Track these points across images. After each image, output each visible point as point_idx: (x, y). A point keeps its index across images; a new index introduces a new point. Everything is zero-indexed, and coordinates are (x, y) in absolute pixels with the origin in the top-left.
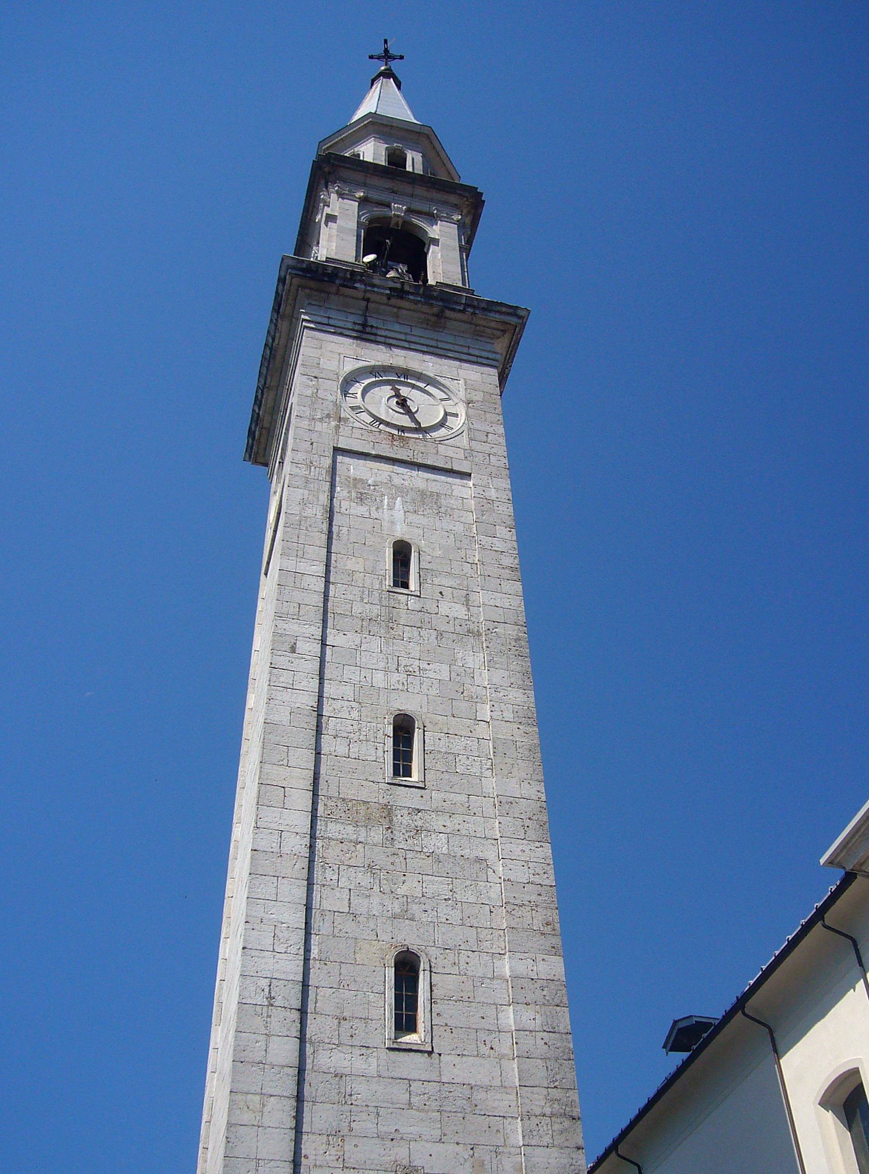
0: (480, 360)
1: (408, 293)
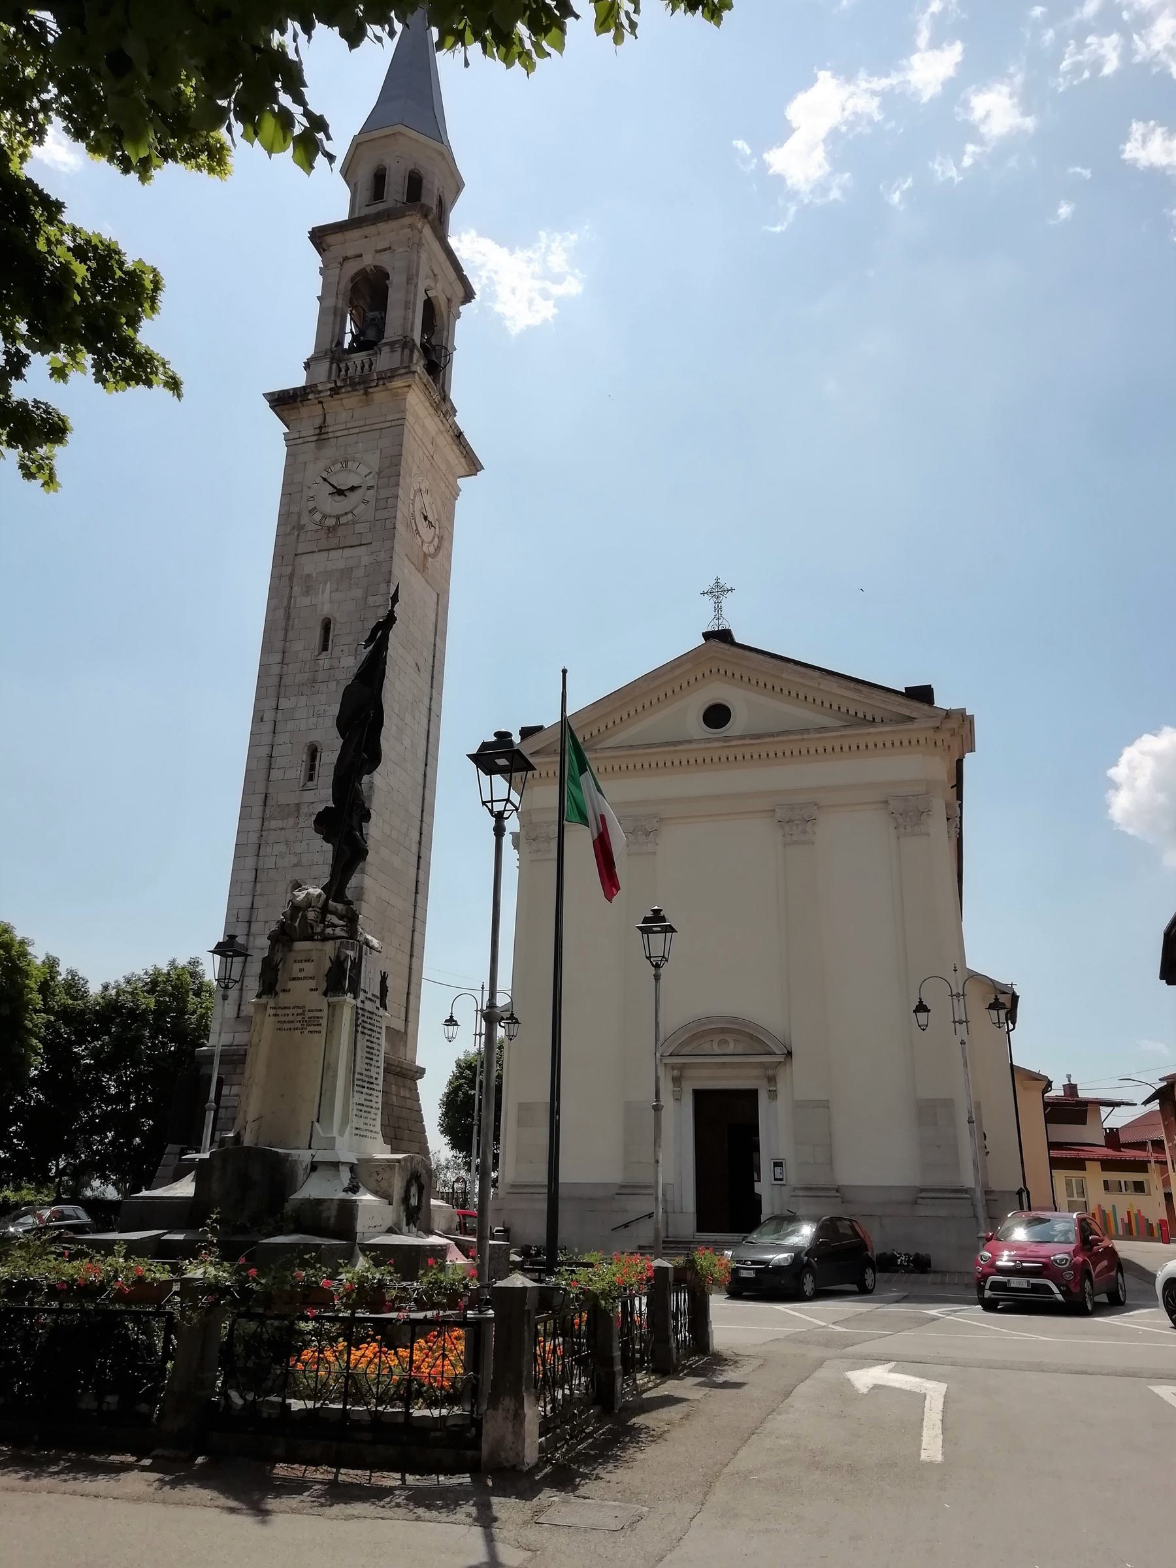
0: (362, 429)
1: (341, 387)
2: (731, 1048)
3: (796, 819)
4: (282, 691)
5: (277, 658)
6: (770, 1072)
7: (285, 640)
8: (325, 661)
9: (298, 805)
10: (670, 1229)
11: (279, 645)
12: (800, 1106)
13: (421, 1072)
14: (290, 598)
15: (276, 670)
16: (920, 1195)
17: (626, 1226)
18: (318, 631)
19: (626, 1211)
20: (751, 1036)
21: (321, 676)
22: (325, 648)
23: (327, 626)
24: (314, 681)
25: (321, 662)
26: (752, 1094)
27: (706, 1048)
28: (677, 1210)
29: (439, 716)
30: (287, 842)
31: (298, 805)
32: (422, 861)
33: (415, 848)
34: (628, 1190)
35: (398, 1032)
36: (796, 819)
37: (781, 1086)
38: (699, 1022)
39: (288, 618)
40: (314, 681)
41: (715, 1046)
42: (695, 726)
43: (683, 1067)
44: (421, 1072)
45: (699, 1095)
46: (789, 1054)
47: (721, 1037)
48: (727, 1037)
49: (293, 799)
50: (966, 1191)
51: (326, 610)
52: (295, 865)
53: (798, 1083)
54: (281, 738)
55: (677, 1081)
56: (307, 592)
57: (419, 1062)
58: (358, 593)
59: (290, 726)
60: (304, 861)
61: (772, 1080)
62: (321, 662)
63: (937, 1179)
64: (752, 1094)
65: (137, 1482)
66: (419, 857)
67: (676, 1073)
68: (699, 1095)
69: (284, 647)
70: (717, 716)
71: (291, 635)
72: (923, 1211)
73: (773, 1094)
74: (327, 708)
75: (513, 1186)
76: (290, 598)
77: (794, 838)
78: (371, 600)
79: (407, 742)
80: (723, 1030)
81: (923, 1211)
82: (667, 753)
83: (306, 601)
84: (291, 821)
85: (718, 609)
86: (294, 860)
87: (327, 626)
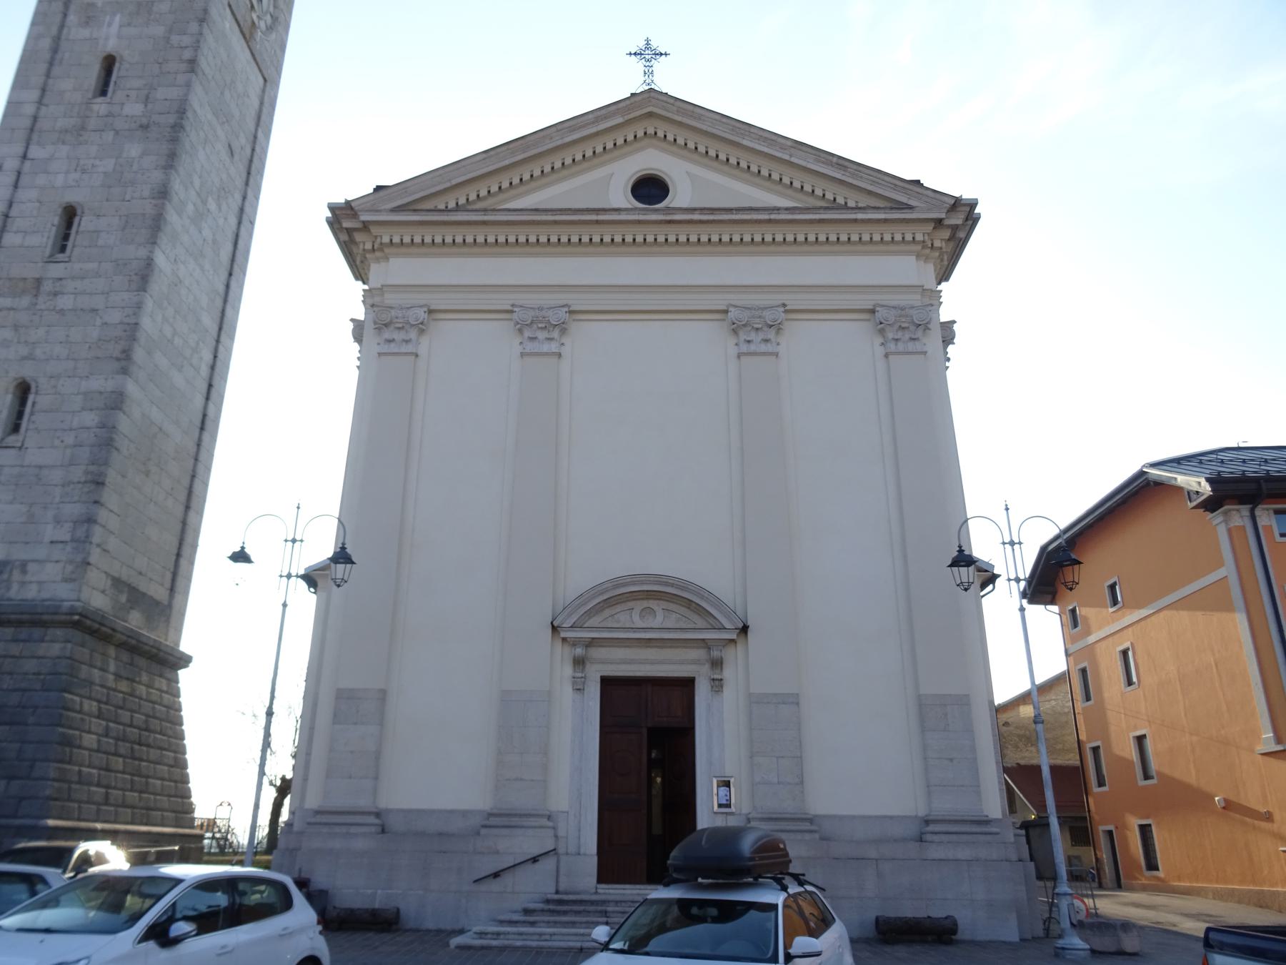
2: (658, 620)
3: (754, 326)
4: (35, 137)
5: (34, 95)
6: (715, 654)
7: (48, 75)
8: (100, 106)
9: (39, 281)
10: (562, 879)
11: (37, 80)
12: (755, 701)
13: (185, 661)
14: (62, 26)
15: (29, 110)
16: (925, 829)
17: (496, 875)
18: (95, 70)
19: (497, 852)
20: (689, 604)
21: (93, 123)
22: (103, 93)
23: (109, 63)
24: (83, 128)
25: (95, 107)
26: (688, 684)
27: (623, 619)
28: (572, 849)
29: (252, 223)
30: (16, 327)
31: (39, 281)
32: (213, 391)
33: (204, 371)
34: (501, 820)
35: (157, 603)
36: (754, 326)
37: (728, 673)
38: (617, 583)
39: (55, 50)
40: (83, 128)
41: (636, 617)
42: (620, 197)
43: (591, 643)
44: (185, 661)
45: (607, 682)
46: (744, 629)
47: (645, 604)
48: (652, 604)
49: (31, 272)
50: (987, 822)
51: (111, 46)
52: (24, 358)
53: (748, 672)
54: (22, 194)
55: (579, 662)
56: (88, 21)
57: (185, 646)
58: (159, 30)
59: (41, 180)
60: (38, 352)
61: (717, 664)
62: (95, 107)
63: (946, 805)
64: (688, 684)
65: (109, 842)
66: (210, 386)
67: (579, 651)
68: (607, 682)
69: (45, 84)
70: (650, 189)
71: (56, 71)
72: (935, 852)
73: (717, 685)
74: (97, 162)
75: (317, 812)
76: (62, 26)
77: (753, 348)
78: (175, 39)
79: (207, 233)
80: (649, 595)
81: (935, 852)
82: (582, 230)
83: (85, 33)
84: (25, 301)
85: (648, 73)
86: (24, 351)
87: (109, 63)
